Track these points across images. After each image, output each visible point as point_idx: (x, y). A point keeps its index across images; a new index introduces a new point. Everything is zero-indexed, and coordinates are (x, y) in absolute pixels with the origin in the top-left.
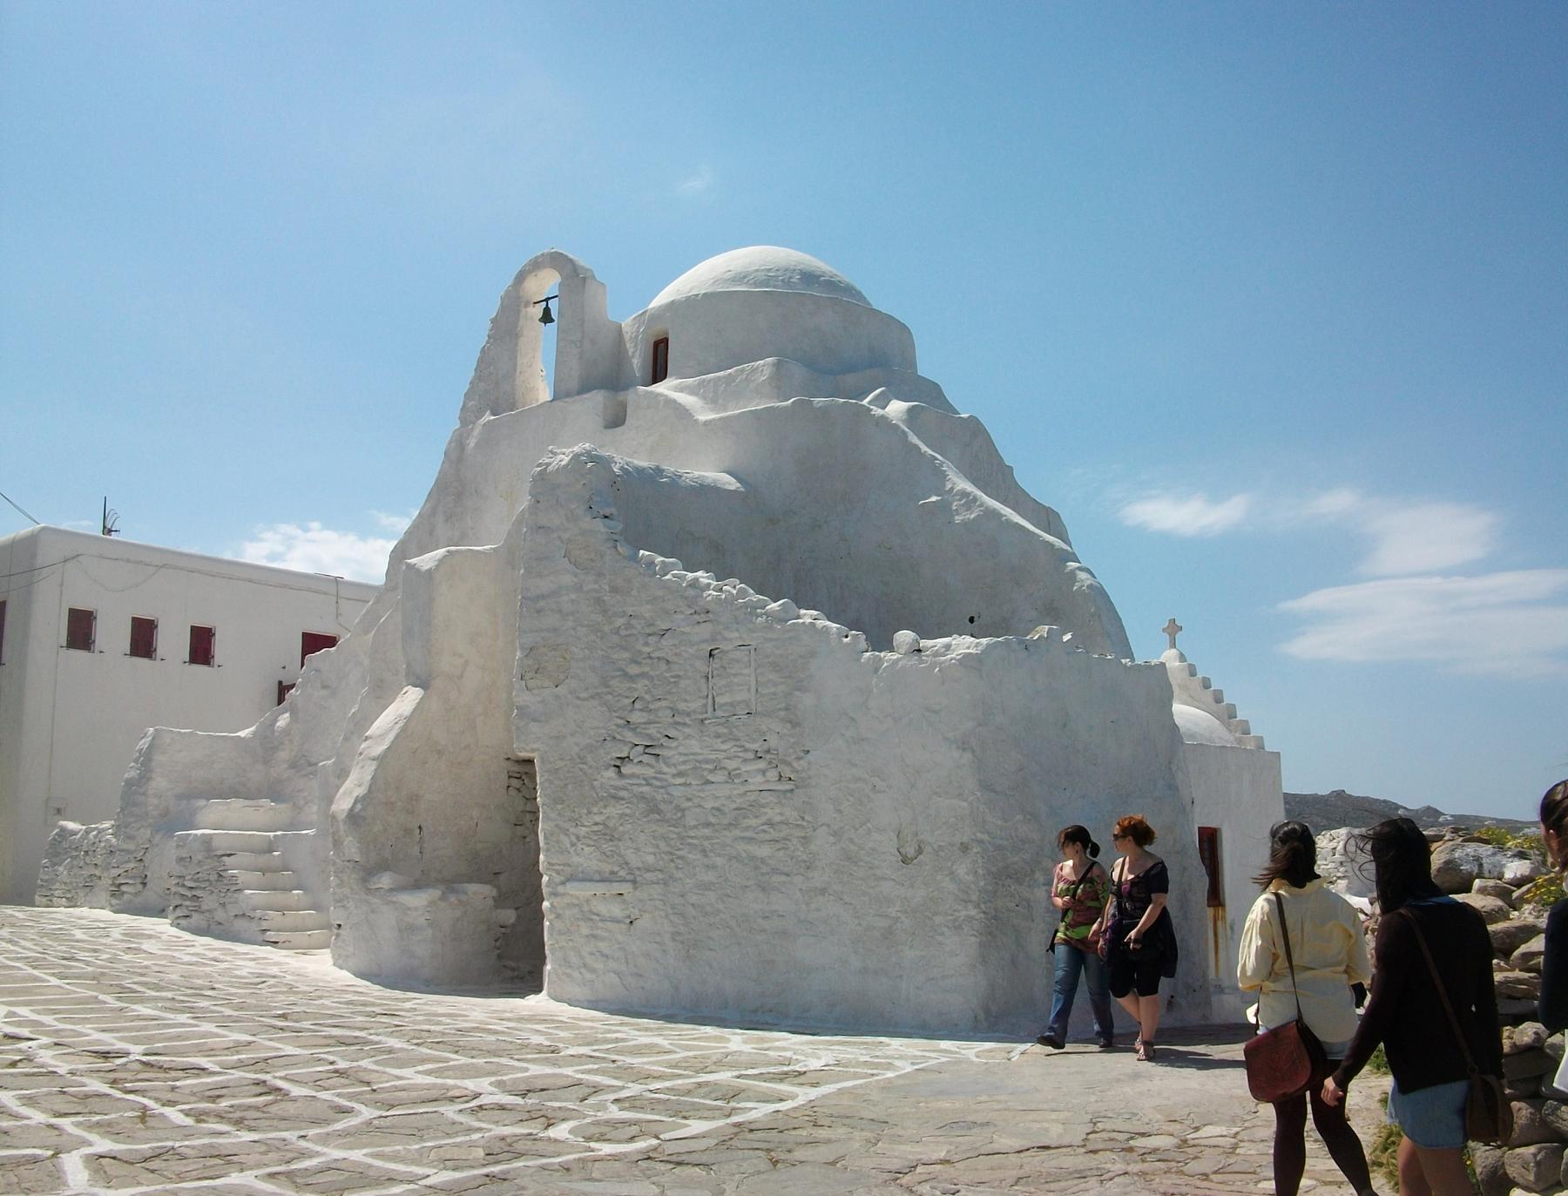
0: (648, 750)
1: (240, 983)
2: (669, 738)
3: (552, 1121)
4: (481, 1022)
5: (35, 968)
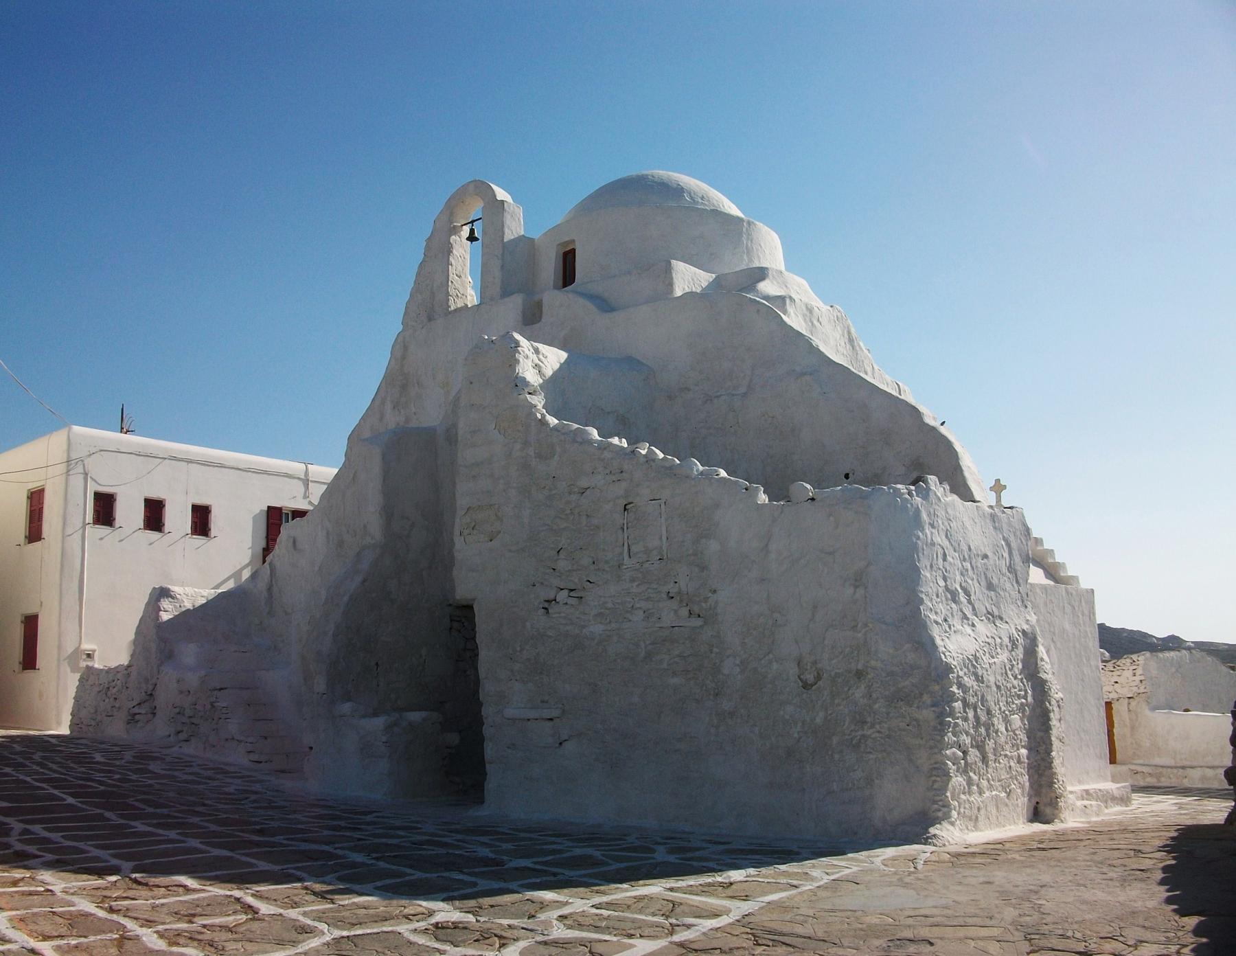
0: (572, 594)
1: (226, 799)
2: (591, 583)
3: (504, 941)
4: (432, 835)
5: (55, 788)
